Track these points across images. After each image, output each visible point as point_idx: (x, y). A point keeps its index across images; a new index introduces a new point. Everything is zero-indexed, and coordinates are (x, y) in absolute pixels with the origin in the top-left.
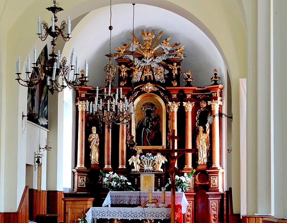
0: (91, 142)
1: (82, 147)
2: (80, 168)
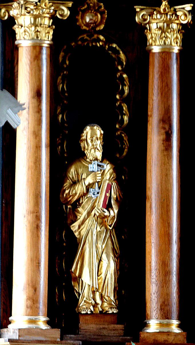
0: (77, 204)
1: (38, 227)
2: (28, 331)
